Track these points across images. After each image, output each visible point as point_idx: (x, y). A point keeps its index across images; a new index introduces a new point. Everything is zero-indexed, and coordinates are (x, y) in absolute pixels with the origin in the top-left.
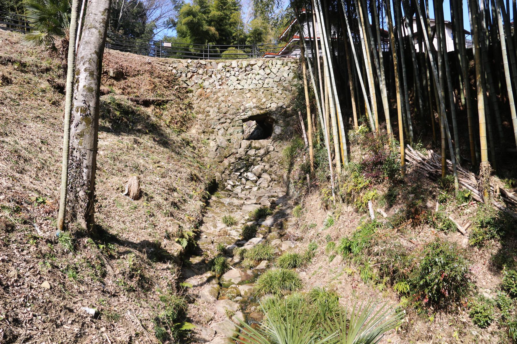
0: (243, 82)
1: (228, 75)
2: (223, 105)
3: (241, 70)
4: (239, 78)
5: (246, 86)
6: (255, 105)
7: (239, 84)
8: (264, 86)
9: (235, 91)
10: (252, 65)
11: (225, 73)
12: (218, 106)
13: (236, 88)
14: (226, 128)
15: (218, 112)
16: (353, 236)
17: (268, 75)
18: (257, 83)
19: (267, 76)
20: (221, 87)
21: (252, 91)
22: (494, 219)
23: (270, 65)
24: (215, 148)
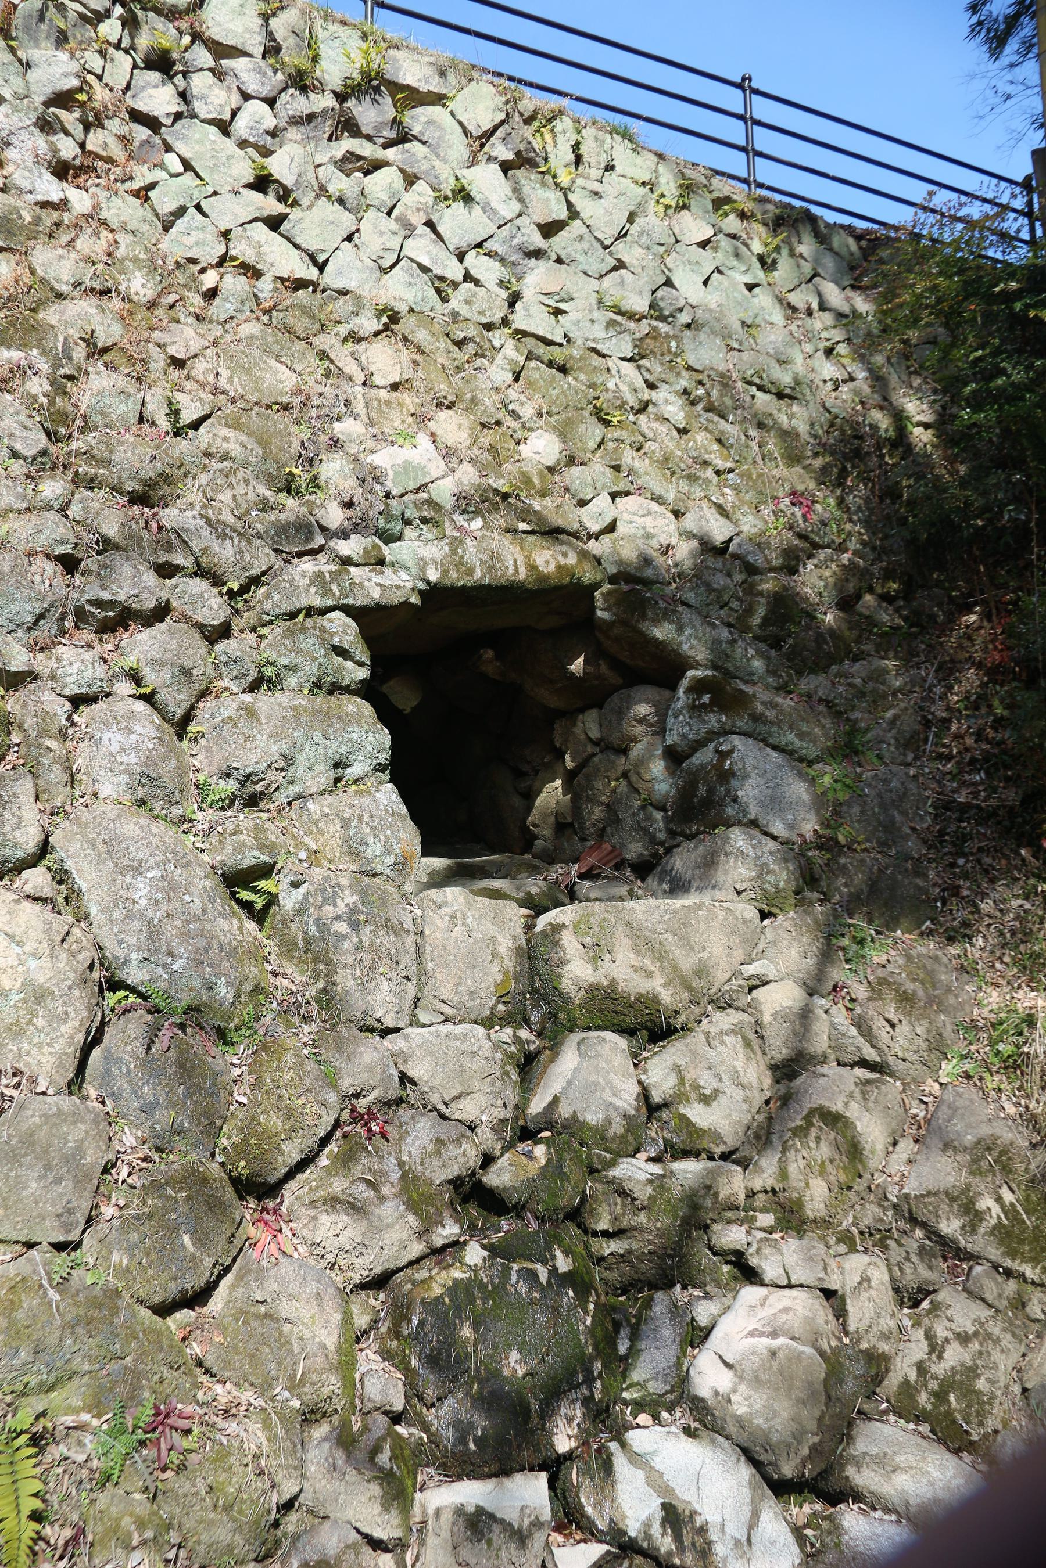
0: (316, 223)
1: (158, 97)
2: (99, 387)
3: (295, 103)
4: (282, 165)
5: (346, 270)
6: (467, 475)
7: (274, 223)
8: (519, 321)
9: (234, 284)
10: (412, 97)
11: (123, 62)
12: (37, 386)
13: (240, 250)
14: (175, 701)
15: (43, 463)
16: (299, 1545)
17: (549, 229)
18: (454, 271)
19: (537, 240)
20: (80, 201)
21: (421, 336)
22: (962, 1365)
23: (560, 155)
24: (71, 1032)
